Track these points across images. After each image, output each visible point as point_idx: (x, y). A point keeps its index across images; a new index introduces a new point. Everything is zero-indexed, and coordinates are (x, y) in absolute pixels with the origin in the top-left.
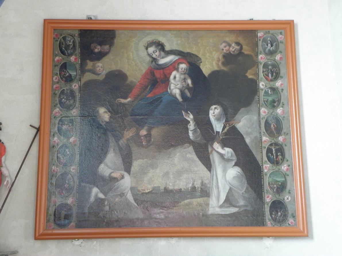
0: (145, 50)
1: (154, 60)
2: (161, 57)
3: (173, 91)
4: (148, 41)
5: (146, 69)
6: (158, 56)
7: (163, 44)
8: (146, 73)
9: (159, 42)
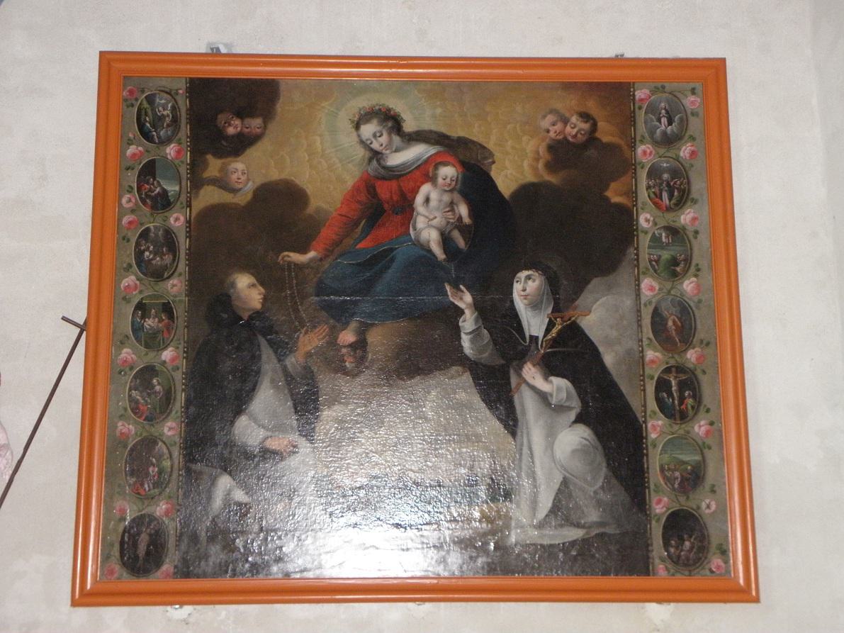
0: (353, 130)
1: (376, 155)
2: (394, 149)
5: (356, 180)
6: (384, 146)
7: (399, 116)
8: (356, 189)
9: (389, 110)
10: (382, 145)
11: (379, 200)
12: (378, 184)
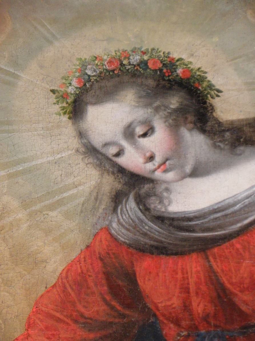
0: (65, 118)
1: (134, 185)
2: (188, 169)
3: (153, 198)
4: (84, 65)
5: (74, 255)
6: (158, 159)
7: (202, 79)
8: (74, 281)
9: (171, 64)
10: (151, 158)
11: (146, 311)
12: (143, 266)
